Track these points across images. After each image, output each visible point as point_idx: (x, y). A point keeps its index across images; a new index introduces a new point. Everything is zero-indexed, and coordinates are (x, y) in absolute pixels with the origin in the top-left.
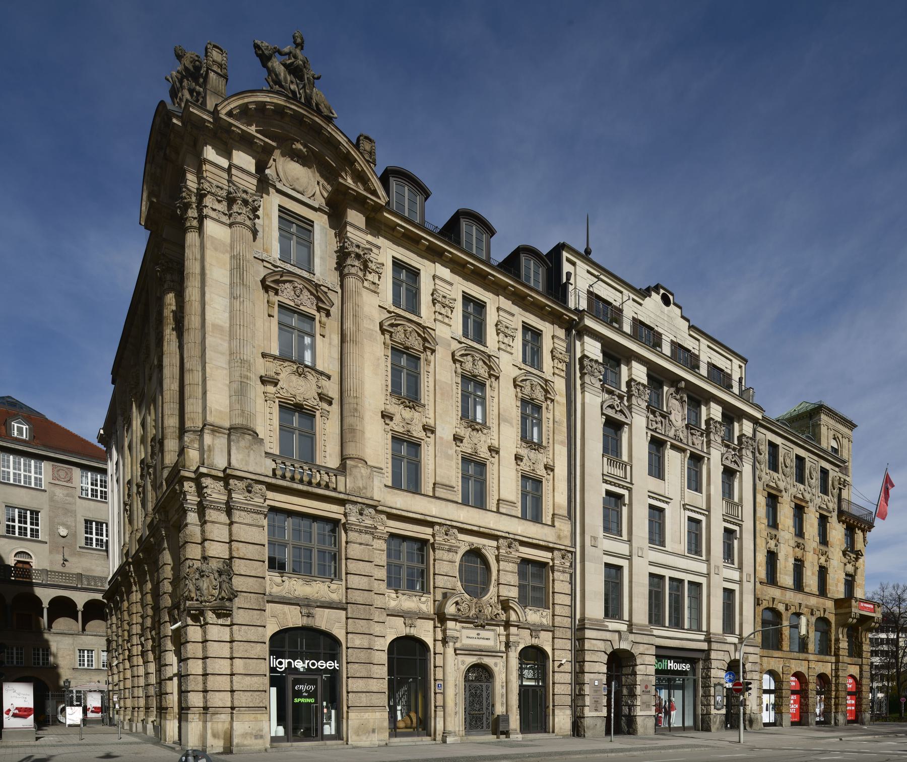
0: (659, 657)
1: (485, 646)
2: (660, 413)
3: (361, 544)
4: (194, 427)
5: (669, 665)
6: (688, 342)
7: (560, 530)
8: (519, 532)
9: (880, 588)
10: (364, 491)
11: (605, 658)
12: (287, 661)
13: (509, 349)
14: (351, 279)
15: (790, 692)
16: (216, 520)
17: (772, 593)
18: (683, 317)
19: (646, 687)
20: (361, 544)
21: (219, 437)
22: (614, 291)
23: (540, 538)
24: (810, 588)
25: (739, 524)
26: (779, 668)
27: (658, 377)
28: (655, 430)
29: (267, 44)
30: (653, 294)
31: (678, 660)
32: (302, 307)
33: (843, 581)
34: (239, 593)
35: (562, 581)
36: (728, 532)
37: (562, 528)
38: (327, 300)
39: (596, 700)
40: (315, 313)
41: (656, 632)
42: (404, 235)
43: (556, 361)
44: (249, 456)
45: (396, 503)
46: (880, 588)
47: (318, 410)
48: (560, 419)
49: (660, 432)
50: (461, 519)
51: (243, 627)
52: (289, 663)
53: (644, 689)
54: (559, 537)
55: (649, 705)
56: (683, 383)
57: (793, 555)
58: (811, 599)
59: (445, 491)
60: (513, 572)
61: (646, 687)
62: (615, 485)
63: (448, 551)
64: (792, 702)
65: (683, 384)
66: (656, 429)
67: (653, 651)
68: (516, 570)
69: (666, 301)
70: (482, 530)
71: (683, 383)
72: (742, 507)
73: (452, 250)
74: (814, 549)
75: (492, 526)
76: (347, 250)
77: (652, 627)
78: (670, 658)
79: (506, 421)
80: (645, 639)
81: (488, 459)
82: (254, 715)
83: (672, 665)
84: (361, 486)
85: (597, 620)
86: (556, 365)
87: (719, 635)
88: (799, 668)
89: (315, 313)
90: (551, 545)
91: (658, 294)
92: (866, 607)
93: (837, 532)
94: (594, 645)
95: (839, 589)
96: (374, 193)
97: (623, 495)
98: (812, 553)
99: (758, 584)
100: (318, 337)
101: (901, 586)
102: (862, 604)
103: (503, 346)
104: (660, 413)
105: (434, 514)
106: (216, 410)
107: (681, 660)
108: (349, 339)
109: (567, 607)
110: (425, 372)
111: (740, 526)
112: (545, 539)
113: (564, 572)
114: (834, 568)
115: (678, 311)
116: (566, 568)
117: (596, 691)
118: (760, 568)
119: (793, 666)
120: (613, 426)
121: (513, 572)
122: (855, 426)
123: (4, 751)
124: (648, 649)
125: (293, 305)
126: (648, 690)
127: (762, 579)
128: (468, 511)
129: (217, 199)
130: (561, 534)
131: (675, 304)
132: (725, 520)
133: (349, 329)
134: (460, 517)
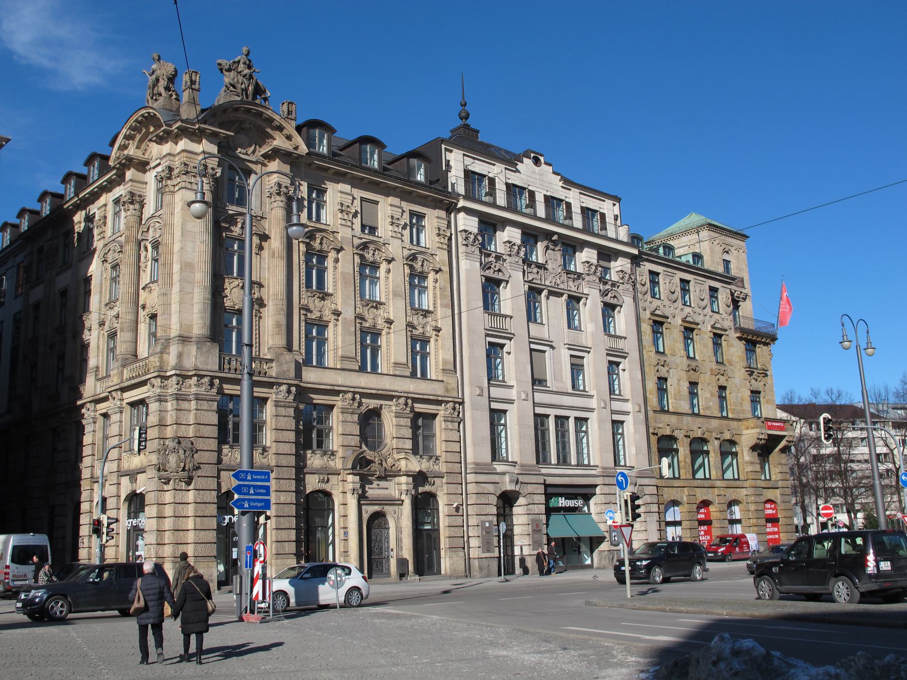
0: (548, 496)
1: (384, 495)
3: (285, 416)
5: (560, 502)
6: (561, 193)
7: (448, 383)
8: (411, 390)
9: (812, 394)
10: (288, 373)
11: (494, 500)
12: (229, 517)
15: (697, 523)
16: (211, 402)
17: (667, 421)
18: (554, 173)
19: (537, 526)
20: (285, 416)
21: (187, 345)
22: (487, 165)
23: (430, 393)
24: (710, 410)
26: (682, 497)
27: (531, 236)
28: (530, 282)
29: (226, 62)
30: (525, 160)
31: (569, 497)
33: (749, 399)
34: (201, 465)
35: (451, 430)
37: (450, 381)
39: (488, 541)
41: (544, 471)
44: (208, 358)
45: (310, 378)
46: (812, 394)
48: (444, 286)
49: (539, 282)
50: (363, 385)
51: (201, 492)
52: (230, 519)
53: (535, 528)
54: (447, 390)
55: (541, 544)
57: (687, 379)
58: (712, 422)
59: (348, 362)
60: (407, 426)
61: (537, 526)
62: (496, 337)
64: (702, 533)
65: (555, 237)
66: (533, 280)
67: (541, 489)
68: (409, 424)
69: (537, 161)
70: (380, 392)
74: (711, 370)
75: (388, 387)
77: (540, 466)
78: (561, 495)
80: (533, 479)
82: (206, 563)
83: (563, 502)
84: (285, 369)
85: (485, 464)
87: (610, 469)
88: (706, 496)
90: (440, 398)
91: (530, 158)
92: (775, 426)
93: (734, 349)
94: (483, 488)
95: (744, 408)
98: (709, 373)
99: (651, 414)
101: (835, 391)
102: (769, 424)
105: (340, 383)
106: (185, 324)
107: (574, 496)
109: (457, 454)
112: (434, 393)
113: (452, 422)
114: (736, 386)
115: (550, 169)
116: (455, 417)
117: (487, 533)
118: (651, 396)
119: (698, 495)
120: (491, 286)
121: (407, 426)
122: (747, 237)
123: (799, 512)
124: (536, 489)
126: (539, 529)
127: (655, 407)
128: (368, 377)
130: (449, 387)
131: (546, 163)
132: (608, 355)
134: (361, 383)
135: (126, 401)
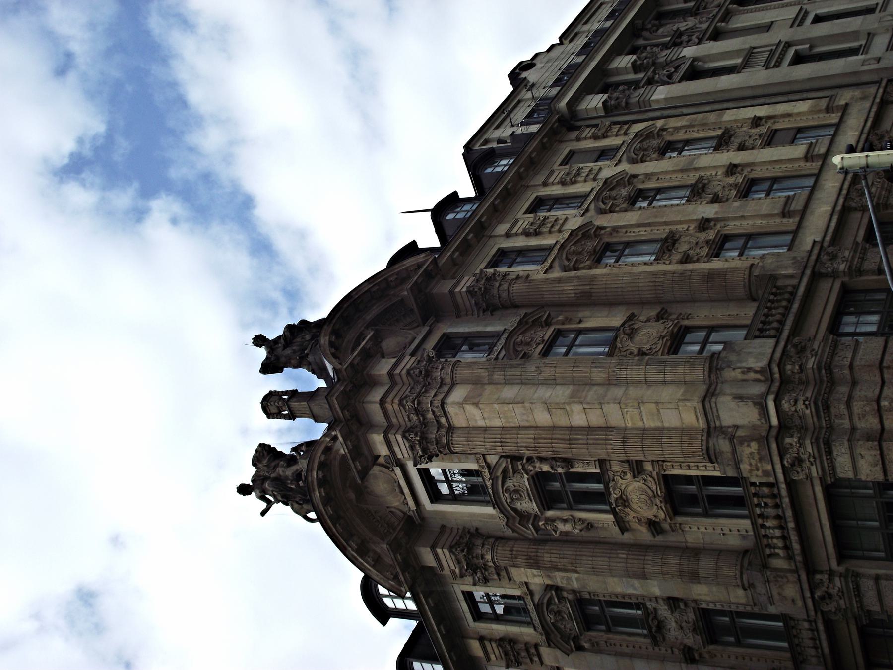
2: (677, 38)
4: (702, 435)
8: (829, 208)
13: (561, 222)
14: (515, 288)
25: (784, 46)
32: (546, 338)
36: (799, 59)
38: (618, 177)
40: (552, 329)
42: (462, 254)
43: (610, 133)
47: (678, 322)
56: (637, 22)
63: (889, 193)
71: (637, 22)
72: (754, 48)
73: (480, 214)
76: (483, 289)
79: (691, 162)
81: (745, 176)
86: (583, 178)
89: (552, 329)
96: (419, 266)
97: (796, 51)
100: (582, 325)
103: (557, 228)
104: (677, 38)
108: (588, 287)
110: (627, 235)
111: (788, 45)
120: (694, 73)
125: (542, 346)
129: (424, 392)
133: (576, 288)
135: (834, 564)
